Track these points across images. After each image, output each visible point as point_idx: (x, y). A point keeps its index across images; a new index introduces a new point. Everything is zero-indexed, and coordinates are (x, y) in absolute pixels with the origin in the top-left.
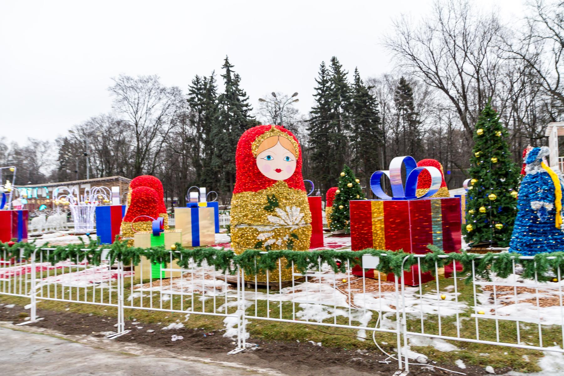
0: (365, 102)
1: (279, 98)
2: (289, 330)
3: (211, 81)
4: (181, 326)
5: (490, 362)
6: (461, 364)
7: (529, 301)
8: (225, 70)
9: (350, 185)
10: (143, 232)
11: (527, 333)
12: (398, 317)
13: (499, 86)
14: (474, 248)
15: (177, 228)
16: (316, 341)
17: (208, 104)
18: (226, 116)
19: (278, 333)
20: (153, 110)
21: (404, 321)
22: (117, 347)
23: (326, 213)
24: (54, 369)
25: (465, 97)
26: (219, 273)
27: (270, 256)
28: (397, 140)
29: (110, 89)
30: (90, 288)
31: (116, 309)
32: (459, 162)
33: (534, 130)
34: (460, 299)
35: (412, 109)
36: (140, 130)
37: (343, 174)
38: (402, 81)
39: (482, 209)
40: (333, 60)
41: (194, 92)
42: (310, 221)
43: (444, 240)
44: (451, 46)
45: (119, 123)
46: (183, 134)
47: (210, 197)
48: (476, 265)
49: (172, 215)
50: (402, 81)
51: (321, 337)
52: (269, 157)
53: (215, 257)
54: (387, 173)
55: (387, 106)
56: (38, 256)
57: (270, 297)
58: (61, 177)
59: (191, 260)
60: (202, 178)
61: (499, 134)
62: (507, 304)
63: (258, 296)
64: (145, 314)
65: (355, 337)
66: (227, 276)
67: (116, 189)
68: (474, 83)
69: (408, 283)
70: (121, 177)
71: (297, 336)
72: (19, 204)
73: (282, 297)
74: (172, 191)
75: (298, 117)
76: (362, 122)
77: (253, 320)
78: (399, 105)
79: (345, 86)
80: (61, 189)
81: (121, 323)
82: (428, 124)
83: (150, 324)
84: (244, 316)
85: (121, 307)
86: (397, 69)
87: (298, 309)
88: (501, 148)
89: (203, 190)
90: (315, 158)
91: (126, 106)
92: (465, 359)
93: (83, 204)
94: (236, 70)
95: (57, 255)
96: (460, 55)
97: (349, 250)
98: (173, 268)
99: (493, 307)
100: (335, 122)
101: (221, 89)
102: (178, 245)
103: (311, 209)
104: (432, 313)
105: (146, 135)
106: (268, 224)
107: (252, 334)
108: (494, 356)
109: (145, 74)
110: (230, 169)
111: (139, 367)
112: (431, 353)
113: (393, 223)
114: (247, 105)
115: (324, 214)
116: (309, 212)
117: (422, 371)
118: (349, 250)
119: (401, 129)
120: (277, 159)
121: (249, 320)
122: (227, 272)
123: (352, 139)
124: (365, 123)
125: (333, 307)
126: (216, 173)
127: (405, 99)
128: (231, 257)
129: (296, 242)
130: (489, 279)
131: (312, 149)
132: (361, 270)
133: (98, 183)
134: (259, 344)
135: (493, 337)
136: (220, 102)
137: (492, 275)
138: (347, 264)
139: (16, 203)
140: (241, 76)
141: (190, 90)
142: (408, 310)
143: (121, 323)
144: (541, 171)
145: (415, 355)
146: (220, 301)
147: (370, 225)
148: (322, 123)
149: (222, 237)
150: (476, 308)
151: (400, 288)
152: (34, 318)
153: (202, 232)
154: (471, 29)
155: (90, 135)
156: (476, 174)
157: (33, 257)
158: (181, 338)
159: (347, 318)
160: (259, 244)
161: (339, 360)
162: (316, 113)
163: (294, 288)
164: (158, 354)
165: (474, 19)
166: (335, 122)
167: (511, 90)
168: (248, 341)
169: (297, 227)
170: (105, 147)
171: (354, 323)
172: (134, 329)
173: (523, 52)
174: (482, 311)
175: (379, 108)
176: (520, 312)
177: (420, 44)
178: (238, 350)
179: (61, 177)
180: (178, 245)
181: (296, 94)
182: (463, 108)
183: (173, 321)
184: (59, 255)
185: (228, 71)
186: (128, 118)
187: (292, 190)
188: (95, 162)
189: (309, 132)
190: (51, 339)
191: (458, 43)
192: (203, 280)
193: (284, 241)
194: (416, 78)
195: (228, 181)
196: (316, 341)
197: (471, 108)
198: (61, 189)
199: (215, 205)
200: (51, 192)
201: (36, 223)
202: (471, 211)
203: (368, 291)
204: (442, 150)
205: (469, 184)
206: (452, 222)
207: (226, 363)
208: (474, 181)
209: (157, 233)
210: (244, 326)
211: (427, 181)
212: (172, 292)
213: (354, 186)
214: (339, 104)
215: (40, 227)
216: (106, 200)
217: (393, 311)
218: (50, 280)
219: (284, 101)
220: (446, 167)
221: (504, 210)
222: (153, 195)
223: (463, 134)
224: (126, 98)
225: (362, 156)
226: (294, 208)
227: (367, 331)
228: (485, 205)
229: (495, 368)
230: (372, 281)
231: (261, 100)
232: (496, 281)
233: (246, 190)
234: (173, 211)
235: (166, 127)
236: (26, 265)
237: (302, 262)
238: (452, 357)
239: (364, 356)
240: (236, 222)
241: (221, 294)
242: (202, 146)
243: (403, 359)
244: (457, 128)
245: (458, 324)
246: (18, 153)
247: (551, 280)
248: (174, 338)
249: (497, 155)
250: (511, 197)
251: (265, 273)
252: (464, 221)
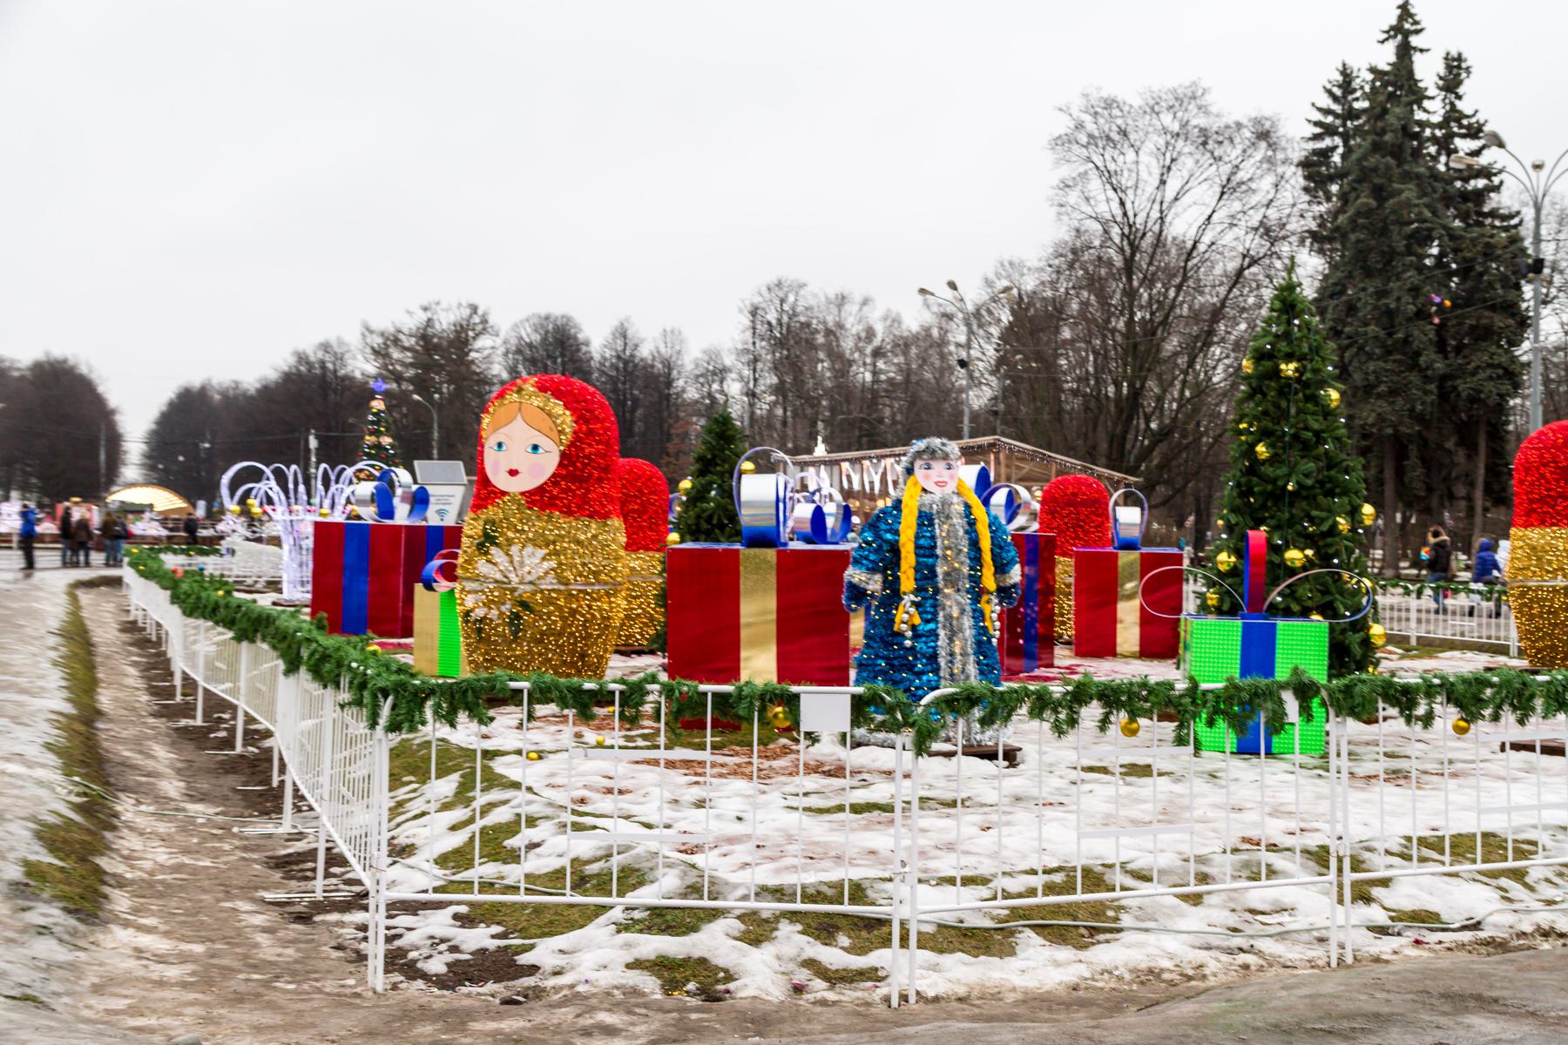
4: (476, 1026)
110: (1370, 420)
140: (1471, 60)
141: (1317, 124)
169: (528, 588)
193: (502, 613)
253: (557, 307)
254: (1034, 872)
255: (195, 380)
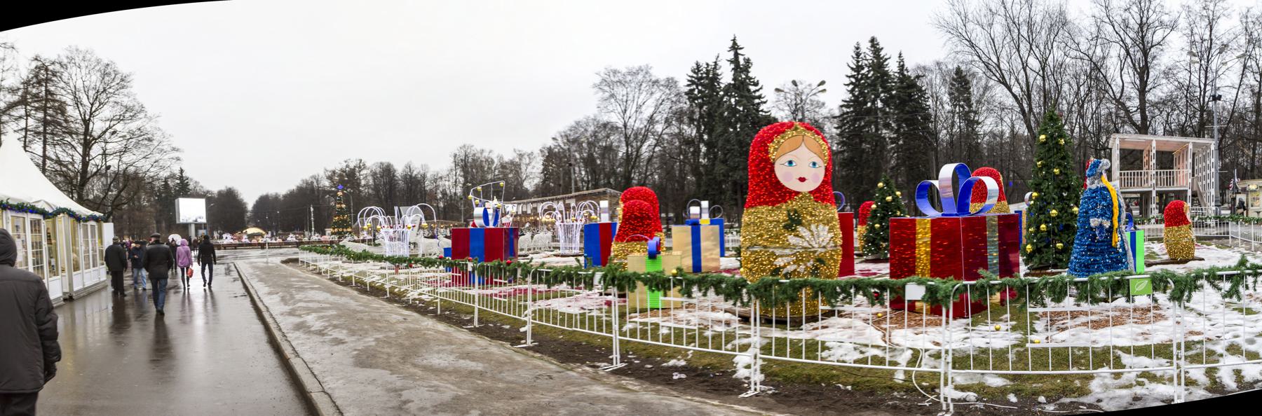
0: (910, 96)
1: (800, 87)
2: (812, 372)
3: (715, 68)
4: (683, 363)
5: (1043, 392)
6: (1013, 398)
7: (1085, 324)
8: (732, 53)
9: (889, 198)
10: (636, 254)
11: (1080, 357)
12: (943, 354)
13: (1066, 87)
14: (1033, 271)
15: (676, 250)
16: (845, 384)
17: (711, 96)
18: (733, 111)
19: (798, 375)
20: (644, 108)
21: (950, 359)
22: (613, 379)
23: (859, 232)
24: (560, 397)
25: (1029, 97)
26: (729, 305)
27: (792, 285)
28: (951, 143)
29: (595, 86)
30: (583, 315)
31: (611, 339)
32: (1022, 173)
33: (1098, 140)
34: (1014, 329)
35: (970, 106)
36: (629, 132)
37: (880, 185)
38: (958, 71)
39: (1043, 226)
40: (873, 40)
41: (693, 83)
42: (840, 242)
43: (1000, 263)
44: (1015, 35)
45: (605, 125)
46: (680, 135)
47: (713, 213)
48: (1031, 291)
49: (669, 236)
50: (958, 71)
51: (851, 380)
52: (790, 162)
53: (723, 286)
54: (936, 183)
55: (940, 101)
56: (534, 277)
57: (791, 335)
58: (544, 191)
59: (695, 289)
60: (703, 189)
61: (1062, 142)
62: (1063, 330)
63: (775, 333)
64: (642, 347)
65: (892, 379)
66: (738, 309)
67: (604, 204)
68: (1039, 81)
69: (959, 314)
70: (609, 190)
71: (823, 379)
72: (507, 220)
73: (804, 334)
74: (667, 205)
75: (824, 112)
76: (905, 121)
77: (769, 360)
78: (954, 100)
79: (886, 74)
80: (545, 205)
81: (616, 355)
82: (988, 125)
83: (648, 359)
84: (759, 356)
85: (616, 337)
86: (952, 56)
87: (825, 348)
88: (1063, 158)
89: (705, 204)
90: (846, 164)
91: (613, 105)
92: (1017, 392)
93: (569, 222)
94: (746, 52)
95: (554, 277)
96: (1024, 47)
97: (888, 278)
98: (674, 297)
99: (1049, 334)
100: (872, 118)
101: (726, 76)
102: (679, 269)
103: (842, 228)
104: (984, 346)
105: (636, 138)
106: (789, 246)
107: (767, 376)
108: (1047, 385)
109: (635, 65)
111: (641, 404)
112: (982, 390)
113: (940, 245)
114: (759, 97)
115: (856, 235)
116: (839, 232)
117: (970, 411)
118: (888, 278)
119: (956, 129)
120: (800, 165)
121: (764, 360)
122: (739, 304)
123: (893, 141)
124: (911, 122)
125: (867, 346)
126: (720, 183)
127: (961, 93)
128: (744, 286)
129: (823, 268)
130: (1044, 306)
131: (842, 152)
132: (903, 302)
133: (584, 197)
134: (776, 387)
135: (1046, 367)
136: (726, 94)
137: (1048, 300)
138: (887, 296)
139: (504, 220)
142: (955, 346)
143: (616, 355)
144: (1101, 185)
145: (959, 395)
146: (730, 337)
147: (913, 247)
148: (855, 120)
149: (729, 262)
150: (1034, 337)
151: (947, 323)
152: (529, 342)
153: (704, 255)
154: (1038, 19)
155: (575, 141)
156: (1037, 188)
157: (529, 279)
158: (683, 376)
159: (884, 359)
160: (776, 271)
161: (871, 404)
162: (847, 106)
163: (819, 324)
164: (658, 392)
165: (1040, 8)
166: (872, 118)
167: (1077, 94)
168: (762, 383)
170: (590, 155)
171: (891, 363)
172: (630, 362)
173: (1091, 52)
174: (1039, 340)
175: (930, 102)
176: (1074, 337)
177: (979, 29)
178: (750, 393)
179: (544, 191)
180: (679, 269)
181: (823, 83)
182: (1027, 110)
183: (674, 357)
184: (555, 277)
185: (736, 55)
186: (616, 119)
187: (819, 205)
188: (581, 173)
189: (838, 131)
190: (550, 366)
191: (1023, 32)
192: (709, 313)
194: (975, 69)
195: (735, 192)
196: (845, 384)
197: (1036, 110)
198: (545, 205)
199: (720, 223)
200: (535, 209)
201: (524, 241)
202: (1031, 230)
203: (909, 326)
204: (1002, 157)
205: (1031, 198)
206: (1010, 242)
207: (736, 407)
208: (1035, 194)
209: (653, 255)
210: (758, 367)
211: (982, 194)
212: (672, 325)
213: (893, 200)
214: (877, 96)
215: (526, 247)
216: (594, 216)
217: (938, 348)
218: (542, 304)
219: (806, 91)
220: (1007, 178)
221: (1065, 228)
222: (648, 210)
223: (1026, 140)
224: (612, 96)
225: (904, 164)
226: (821, 226)
227: (905, 372)
228: (1046, 222)
229: (1047, 397)
230: (913, 315)
231: (777, 90)
232: (1051, 306)
233: (760, 204)
234: (669, 230)
235: (659, 128)
236: (523, 287)
237: (830, 293)
238: (1003, 391)
239: (901, 399)
240: (747, 243)
241: (730, 329)
242: (704, 149)
243: (946, 399)
244: (1021, 132)
245: (1011, 356)
246: (503, 166)
247: (1106, 301)
248: (676, 376)
249: (1059, 165)
250: (1072, 214)
251: (784, 306)
252: (1024, 241)
253: (385, 160)
254: (823, 327)
255: (264, 193)
